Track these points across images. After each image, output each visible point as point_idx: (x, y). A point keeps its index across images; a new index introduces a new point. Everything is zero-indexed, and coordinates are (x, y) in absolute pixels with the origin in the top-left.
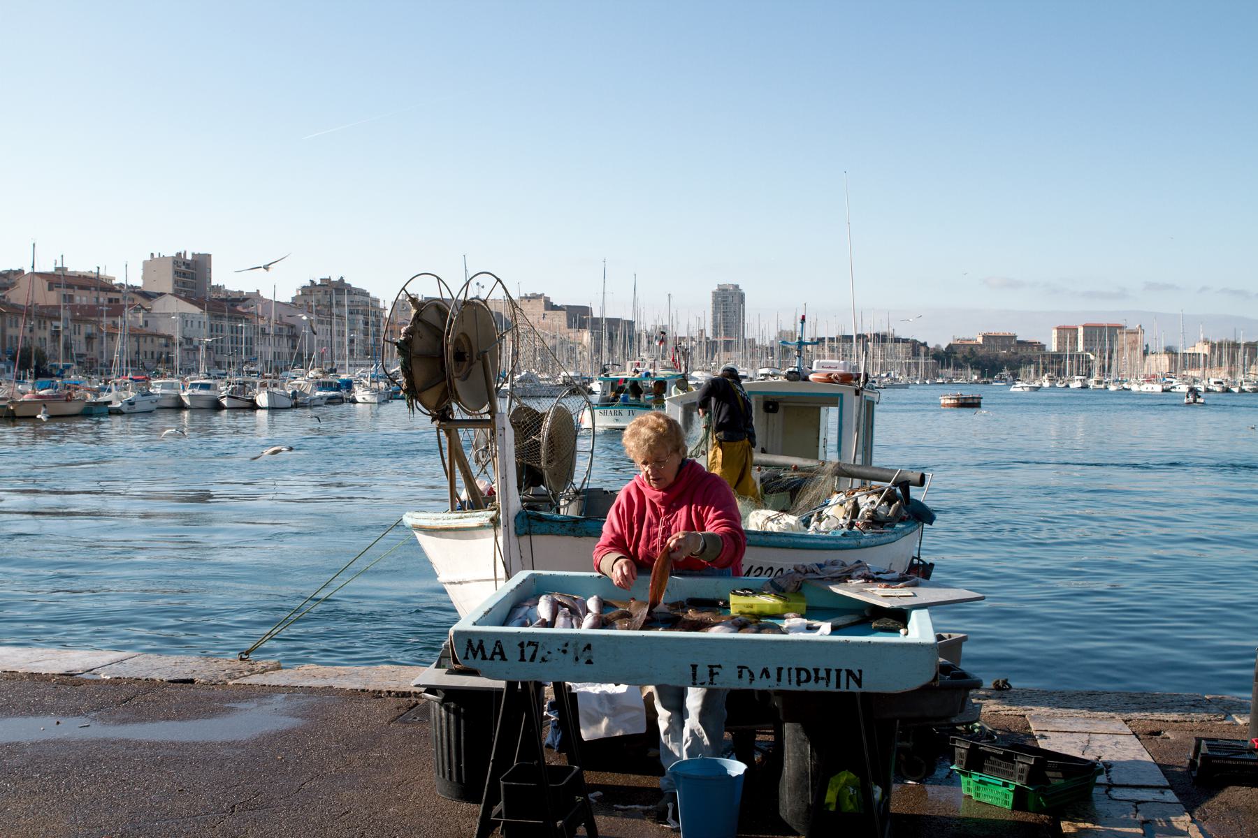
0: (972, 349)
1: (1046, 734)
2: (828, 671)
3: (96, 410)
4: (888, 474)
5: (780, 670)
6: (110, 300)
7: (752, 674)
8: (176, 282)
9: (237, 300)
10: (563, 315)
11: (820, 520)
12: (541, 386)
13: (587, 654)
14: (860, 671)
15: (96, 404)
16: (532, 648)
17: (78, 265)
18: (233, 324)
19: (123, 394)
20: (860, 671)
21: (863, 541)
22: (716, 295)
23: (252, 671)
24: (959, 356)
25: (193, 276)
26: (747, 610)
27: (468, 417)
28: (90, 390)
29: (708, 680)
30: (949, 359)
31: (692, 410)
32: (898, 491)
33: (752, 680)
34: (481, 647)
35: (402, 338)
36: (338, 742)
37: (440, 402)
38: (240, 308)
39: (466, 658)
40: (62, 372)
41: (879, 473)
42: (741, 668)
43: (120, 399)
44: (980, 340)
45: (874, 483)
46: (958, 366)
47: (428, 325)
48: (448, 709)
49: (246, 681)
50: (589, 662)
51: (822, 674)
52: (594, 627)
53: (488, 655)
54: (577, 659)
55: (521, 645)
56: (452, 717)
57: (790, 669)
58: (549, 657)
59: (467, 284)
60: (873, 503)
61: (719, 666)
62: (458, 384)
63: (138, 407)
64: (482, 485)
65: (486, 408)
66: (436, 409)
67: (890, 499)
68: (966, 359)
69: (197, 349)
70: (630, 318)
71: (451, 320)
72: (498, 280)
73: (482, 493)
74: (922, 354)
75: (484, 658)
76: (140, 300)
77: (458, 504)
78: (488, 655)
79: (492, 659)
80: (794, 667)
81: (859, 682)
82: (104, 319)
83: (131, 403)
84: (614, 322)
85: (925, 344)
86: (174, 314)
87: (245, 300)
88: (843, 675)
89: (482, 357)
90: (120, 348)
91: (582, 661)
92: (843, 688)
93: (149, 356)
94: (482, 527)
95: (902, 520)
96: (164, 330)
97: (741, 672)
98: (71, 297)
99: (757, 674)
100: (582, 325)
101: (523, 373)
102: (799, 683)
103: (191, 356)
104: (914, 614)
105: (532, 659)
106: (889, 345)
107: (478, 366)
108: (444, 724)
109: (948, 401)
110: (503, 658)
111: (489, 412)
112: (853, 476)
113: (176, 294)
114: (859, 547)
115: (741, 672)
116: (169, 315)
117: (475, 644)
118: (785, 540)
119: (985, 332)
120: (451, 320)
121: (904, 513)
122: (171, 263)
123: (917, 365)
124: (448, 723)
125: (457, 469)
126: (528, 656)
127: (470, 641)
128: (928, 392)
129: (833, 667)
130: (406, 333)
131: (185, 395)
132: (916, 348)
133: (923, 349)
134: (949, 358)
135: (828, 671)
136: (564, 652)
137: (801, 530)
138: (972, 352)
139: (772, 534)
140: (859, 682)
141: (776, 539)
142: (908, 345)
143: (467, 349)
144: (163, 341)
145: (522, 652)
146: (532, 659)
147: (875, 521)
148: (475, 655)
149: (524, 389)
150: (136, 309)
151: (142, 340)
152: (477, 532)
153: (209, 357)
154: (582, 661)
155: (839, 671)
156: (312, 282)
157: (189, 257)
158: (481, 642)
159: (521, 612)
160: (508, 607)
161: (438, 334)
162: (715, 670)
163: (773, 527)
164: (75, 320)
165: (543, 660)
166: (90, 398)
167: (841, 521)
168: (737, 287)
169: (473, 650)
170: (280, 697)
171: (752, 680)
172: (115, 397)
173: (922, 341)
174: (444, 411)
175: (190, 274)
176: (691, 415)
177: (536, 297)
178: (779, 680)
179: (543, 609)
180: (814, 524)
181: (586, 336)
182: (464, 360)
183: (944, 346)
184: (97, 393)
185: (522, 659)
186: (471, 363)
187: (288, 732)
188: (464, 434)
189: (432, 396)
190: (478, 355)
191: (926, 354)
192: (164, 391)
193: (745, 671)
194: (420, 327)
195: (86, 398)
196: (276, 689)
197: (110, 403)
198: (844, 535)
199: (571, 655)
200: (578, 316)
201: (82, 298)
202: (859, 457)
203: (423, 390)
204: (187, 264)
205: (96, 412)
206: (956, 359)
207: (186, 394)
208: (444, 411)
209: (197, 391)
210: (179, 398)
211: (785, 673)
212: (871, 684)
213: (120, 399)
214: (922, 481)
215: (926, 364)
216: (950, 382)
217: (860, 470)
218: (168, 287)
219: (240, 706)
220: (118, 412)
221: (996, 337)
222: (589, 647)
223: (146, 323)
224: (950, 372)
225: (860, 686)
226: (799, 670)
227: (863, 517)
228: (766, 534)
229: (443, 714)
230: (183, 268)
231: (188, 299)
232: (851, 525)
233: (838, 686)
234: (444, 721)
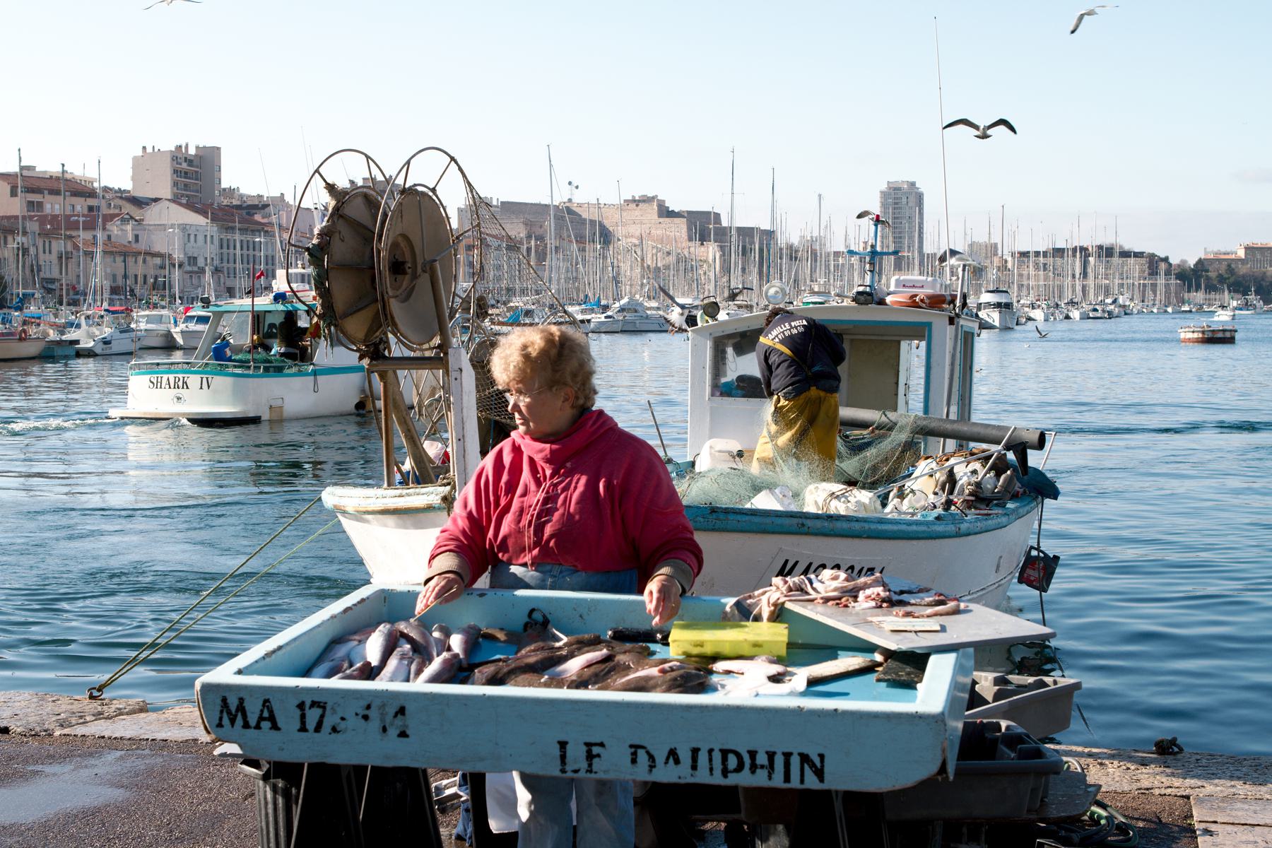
0: (1231, 265)
1: (1213, 827)
2: (771, 756)
3: (59, 351)
4: (994, 433)
5: (695, 751)
6: (91, 209)
7: (651, 758)
8: (175, 184)
9: (255, 207)
10: (682, 224)
11: (901, 496)
12: (647, 317)
13: (399, 721)
14: (822, 756)
15: (60, 343)
16: (318, 712)
17: (47, 164)
18: (249, 238)
19: (95, 330)
20: (822, 756)
21: (964, 527)
22: (884, 195)
23: (99, 716)
24: (1212, 274)
25: (197, 176)
26: (696, 651)
27: (412, 354)
28: (53, 325)
29: (584, 765)
30: (1200, 278)
31: (725, 345)
32: (1011, 456)
33: (652, 767)
34: (241, 708)
35: (315, 241)
36: (159, 828)
37: (371, 331)
38: (258, 217)
39: (220, 725)
40: (22, 301)
41: (983, 431)
42: (636, 747)
43: (92, 336)
44: (1241, 254)
45: (972, 444)
46: (1211, 288)
47: (355, 225)
48: (275, 789)
49: (80, 730)
50: (403, 734)
51: (762, 759)
52: (435, 679)
53: (253, 721)
54: (384, 729)
55: (301, 706)
56: (280, 800)
57: (711, 751)
58: (342, 725)
59: (408, 163)
60: (974, 472)
61: (602, 745)
62: (395, 307)
63: (115, 347)
64: (432, 449)
65: (437, 341)
66: (364, 342)
67: (999, 467)
68: (1222, 279)
69: (202, 271)
70: (766, 226)
71: (385, 215)
72: (453, 159)
73: (431, 461)
74: (1162, 273)
75: (246, 725)
76: (128, 208)
77: (398, 477)
78: (253, 721)
79: (258, 727)
80: (717, 748)
81: (820, 774)
82: (81, 233)
83: (106, 342)
84: (746, 233)
85: (1166, 260)
86: (172, 226)
87: (266, 206)
88: (795, 761)
89: (430, 268)
90: (99, 273)
91: (393, 732)
92: (795, 783)
93: (140, 279)
94: (430, 508)
95: (1015, 497)
96: (159, 247)
97: (634, 754)
98: (40, 204)
99: (660, 757)
100: (703, 239)
101: (625, 301)
102: (725, 773)
103: (195, 281)
104: (933, 659)
105: (318, 728)
106: (1116, 260)
107: (424, 280)
108: (270, 811)
109: (1190, 335)
110: (275, 727)
111: (440, 347)
112: (946, 435)
113: (175, 200)
114: (959, 535)
115: (634, 754)
116: (163, 227)
117: (233, 703)
118: (857, 526)
119: (1249, 242)
120: (385, 215)
121: (1017, 487)
122: (169, 159)
123: (1154, 286)
124: (275, 809)
125: (397, 426)
126: (311, 723)
127: (224, 700)
128: (1166, 323)
129: (780, 750)
130: (321, 235)
131: (176, 332)
132: (1154, 263)
133: (1163, 266)
134: (1198, 278)
135: (771, 756)
136: (366, 718)
137: (875, 511)
138: (1230, 269)
139: (838, 518)
140: (820, 774)
141: (845, 525)
142: (1143, 261)
143: (408, 257)
144: (158, 261)
145: (303, 717)
146: (318, 728)
147: (979, 498)
148: (233, 722)
149: (625, 322)
150: (123, 220)
151: (131, 260)
152: (421, 516)
153: (218, 282)
154: (393, 732)
155: (787, 756)
156: (352, 182)
157: (192, 151)
158: (241, 700)
159: (341, 651)
160: (324, 642)
161: (365, 235)
162: (595, 750)
163: (838, 508)
164: (44, 234)
165: (334, 730)
166: (53, 335)
167: (932, 498)
168: (913, 184)
169: (229, 713)
170: (112, 756)
171: (652, 767)
172: (85, 336)
173: (1163, 255)
174: (376, 345)
175: (194, 174)
176: (724, 352)
177: (646, 200)
178: (694, 767)
179: (373, 648)
180: (893, 502)
181: (711, 251)
182: (404, 273)
183: (1192, 262)
184: (62, 329)
185: (303, 729)
186: (415, 277)
187: (95, 812)
188: (404, 376)
189: (357, 325)
190: (424, 265)
191: (1168, 273)
192: (150, 326)
193: (641, 753)
194: (341, 225)
195: (46, 334)
196: (114, 743)
197: (77, 342)
198: (938, 518)
199: (375, 724)
200: (703, 226)
201: (53, 206)
202: (954, 409)
203: (346, 315)
204: (189, 161)
205: (61, 353)
206: (1208, 278)
207: (178, 329)
208: (376, 345)
209: (193, 326)
210: (169, 335)
211: (703, 758)
212: (839, 779)
213: (92, 336)
214: (1041, 444)
215: (1167, 286)
216: (1200, 309)
217: (956, 427)
218: (165, 191)
219: (48, 769)
220: (89, 354)
221: (1262, 250)
222: (402, 711)
223: (137, 237)
224: (1199, 296)
225: (822, 780)
226: (725, 753)
227: (962, 492)
228: (830, 518)
229: (269, 796)
230: (184, 165)
231: (190, 206)
232: (948, 504)
233: (787, 779)
234: (270, 806)
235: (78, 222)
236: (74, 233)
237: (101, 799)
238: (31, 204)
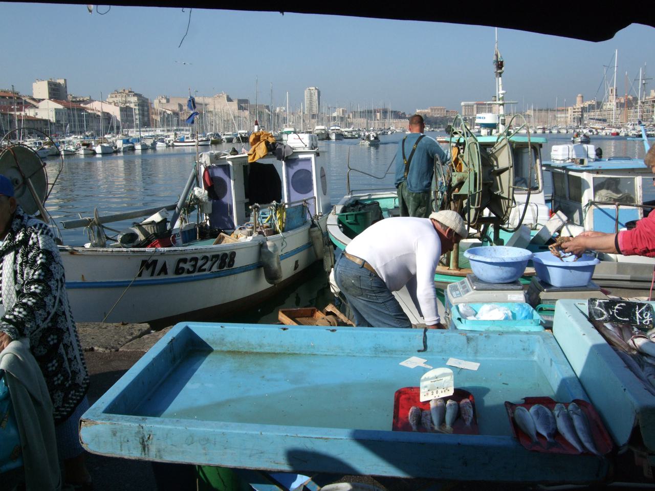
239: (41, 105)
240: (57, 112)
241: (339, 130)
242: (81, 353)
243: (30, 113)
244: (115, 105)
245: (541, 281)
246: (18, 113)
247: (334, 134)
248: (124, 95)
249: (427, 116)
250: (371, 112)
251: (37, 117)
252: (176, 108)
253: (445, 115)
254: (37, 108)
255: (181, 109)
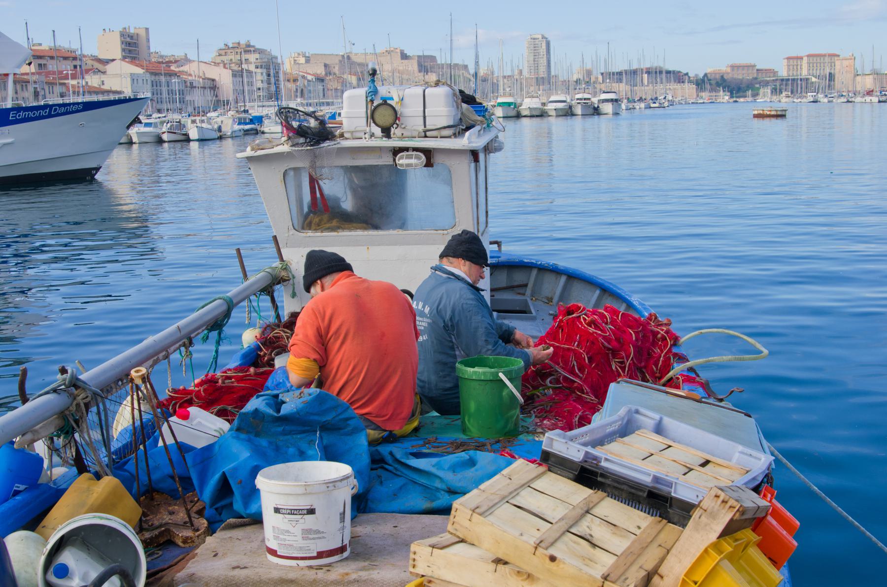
8: (123, 50)
9: (170, 62)
17: (46, 44)
76: (97, 65)
183: (701, 76)
235: (67, 74)
236: (66, 81)
237: (460, 484)
238: (40, 65)
239: (109, 68)
240: (134, 78)
241: (589, 99)
242: (113, 385)
243: (93, 81)
244: (225, 67)
245: (92, 180)
246: (74, 82)
247: (580, 106)
248: (239, 51)
249: (725, 77)
250: (661, 72)
251: (102, 87)
252: (321, 71)
253: (755, 76)
254: (104, 73)
255: (328, 73)
